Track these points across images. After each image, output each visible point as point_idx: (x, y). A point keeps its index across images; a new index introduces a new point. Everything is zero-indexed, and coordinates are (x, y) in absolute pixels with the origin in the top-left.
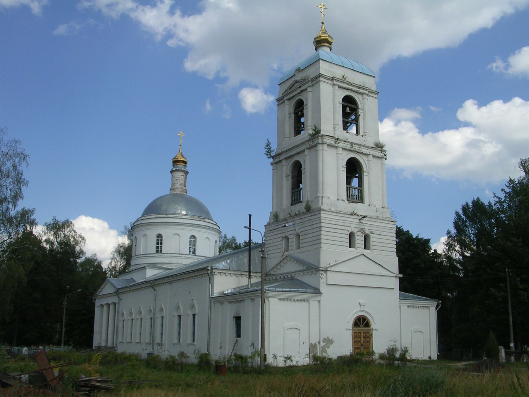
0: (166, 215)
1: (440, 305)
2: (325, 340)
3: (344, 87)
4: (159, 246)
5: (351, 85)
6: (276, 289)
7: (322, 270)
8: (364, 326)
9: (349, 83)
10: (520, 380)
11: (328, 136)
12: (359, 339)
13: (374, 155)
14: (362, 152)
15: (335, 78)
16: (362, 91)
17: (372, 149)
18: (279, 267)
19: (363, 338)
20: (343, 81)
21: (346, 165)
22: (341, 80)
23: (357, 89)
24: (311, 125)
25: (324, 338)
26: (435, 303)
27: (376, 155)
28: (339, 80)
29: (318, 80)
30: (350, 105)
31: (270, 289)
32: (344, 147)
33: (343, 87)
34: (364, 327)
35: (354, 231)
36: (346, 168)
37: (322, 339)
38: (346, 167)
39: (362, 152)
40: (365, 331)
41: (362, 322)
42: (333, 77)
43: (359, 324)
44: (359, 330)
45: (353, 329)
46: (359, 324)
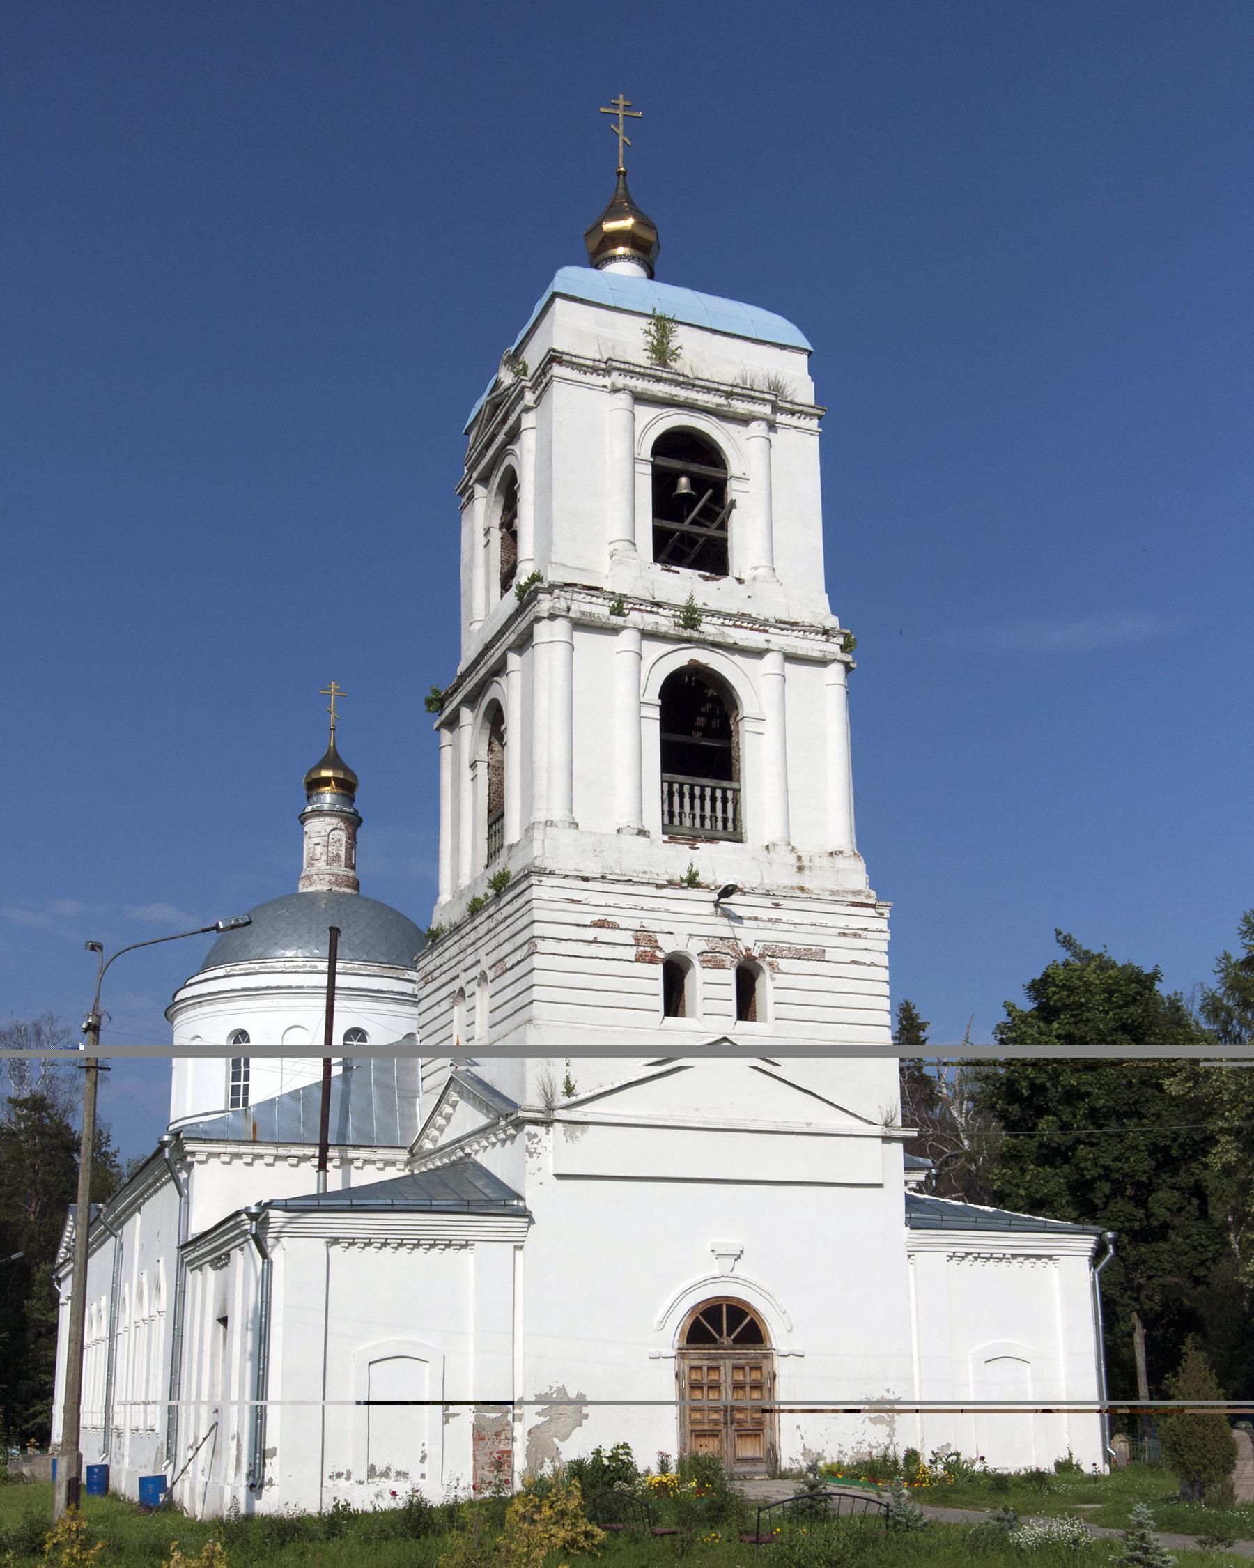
0: (263, 965)
3: (660, 394)
4: (242, 1083)
5: (694, 386)
6: (355, 1202)
7: (535, 1122)
8: (736, 1341)
9: (681, 379)
10: (60, 1494)
13: (791, 650)
14: (731, 641)
15: (615, 364)
16: (741, 407)
17: (782, 629)
18: (440, 1121)
19: (730, 1392)
20: (653, 372)
21: (659, 698)
22: (642, 370)
23: (722, 401)
24: (532, 557)
26: (1087, 1243)
28: (637, 370)
29: (548, 376)
30: (695, 468)
31: (322, 1202)
32: (648, 628)
34: (739, 1346)
36: (661, 707)
38: (659, 702)
40: (743, 1361)
41: (725, 1326)
42: (610, 359)
44: (711, 1357)
45: (682, 1355)
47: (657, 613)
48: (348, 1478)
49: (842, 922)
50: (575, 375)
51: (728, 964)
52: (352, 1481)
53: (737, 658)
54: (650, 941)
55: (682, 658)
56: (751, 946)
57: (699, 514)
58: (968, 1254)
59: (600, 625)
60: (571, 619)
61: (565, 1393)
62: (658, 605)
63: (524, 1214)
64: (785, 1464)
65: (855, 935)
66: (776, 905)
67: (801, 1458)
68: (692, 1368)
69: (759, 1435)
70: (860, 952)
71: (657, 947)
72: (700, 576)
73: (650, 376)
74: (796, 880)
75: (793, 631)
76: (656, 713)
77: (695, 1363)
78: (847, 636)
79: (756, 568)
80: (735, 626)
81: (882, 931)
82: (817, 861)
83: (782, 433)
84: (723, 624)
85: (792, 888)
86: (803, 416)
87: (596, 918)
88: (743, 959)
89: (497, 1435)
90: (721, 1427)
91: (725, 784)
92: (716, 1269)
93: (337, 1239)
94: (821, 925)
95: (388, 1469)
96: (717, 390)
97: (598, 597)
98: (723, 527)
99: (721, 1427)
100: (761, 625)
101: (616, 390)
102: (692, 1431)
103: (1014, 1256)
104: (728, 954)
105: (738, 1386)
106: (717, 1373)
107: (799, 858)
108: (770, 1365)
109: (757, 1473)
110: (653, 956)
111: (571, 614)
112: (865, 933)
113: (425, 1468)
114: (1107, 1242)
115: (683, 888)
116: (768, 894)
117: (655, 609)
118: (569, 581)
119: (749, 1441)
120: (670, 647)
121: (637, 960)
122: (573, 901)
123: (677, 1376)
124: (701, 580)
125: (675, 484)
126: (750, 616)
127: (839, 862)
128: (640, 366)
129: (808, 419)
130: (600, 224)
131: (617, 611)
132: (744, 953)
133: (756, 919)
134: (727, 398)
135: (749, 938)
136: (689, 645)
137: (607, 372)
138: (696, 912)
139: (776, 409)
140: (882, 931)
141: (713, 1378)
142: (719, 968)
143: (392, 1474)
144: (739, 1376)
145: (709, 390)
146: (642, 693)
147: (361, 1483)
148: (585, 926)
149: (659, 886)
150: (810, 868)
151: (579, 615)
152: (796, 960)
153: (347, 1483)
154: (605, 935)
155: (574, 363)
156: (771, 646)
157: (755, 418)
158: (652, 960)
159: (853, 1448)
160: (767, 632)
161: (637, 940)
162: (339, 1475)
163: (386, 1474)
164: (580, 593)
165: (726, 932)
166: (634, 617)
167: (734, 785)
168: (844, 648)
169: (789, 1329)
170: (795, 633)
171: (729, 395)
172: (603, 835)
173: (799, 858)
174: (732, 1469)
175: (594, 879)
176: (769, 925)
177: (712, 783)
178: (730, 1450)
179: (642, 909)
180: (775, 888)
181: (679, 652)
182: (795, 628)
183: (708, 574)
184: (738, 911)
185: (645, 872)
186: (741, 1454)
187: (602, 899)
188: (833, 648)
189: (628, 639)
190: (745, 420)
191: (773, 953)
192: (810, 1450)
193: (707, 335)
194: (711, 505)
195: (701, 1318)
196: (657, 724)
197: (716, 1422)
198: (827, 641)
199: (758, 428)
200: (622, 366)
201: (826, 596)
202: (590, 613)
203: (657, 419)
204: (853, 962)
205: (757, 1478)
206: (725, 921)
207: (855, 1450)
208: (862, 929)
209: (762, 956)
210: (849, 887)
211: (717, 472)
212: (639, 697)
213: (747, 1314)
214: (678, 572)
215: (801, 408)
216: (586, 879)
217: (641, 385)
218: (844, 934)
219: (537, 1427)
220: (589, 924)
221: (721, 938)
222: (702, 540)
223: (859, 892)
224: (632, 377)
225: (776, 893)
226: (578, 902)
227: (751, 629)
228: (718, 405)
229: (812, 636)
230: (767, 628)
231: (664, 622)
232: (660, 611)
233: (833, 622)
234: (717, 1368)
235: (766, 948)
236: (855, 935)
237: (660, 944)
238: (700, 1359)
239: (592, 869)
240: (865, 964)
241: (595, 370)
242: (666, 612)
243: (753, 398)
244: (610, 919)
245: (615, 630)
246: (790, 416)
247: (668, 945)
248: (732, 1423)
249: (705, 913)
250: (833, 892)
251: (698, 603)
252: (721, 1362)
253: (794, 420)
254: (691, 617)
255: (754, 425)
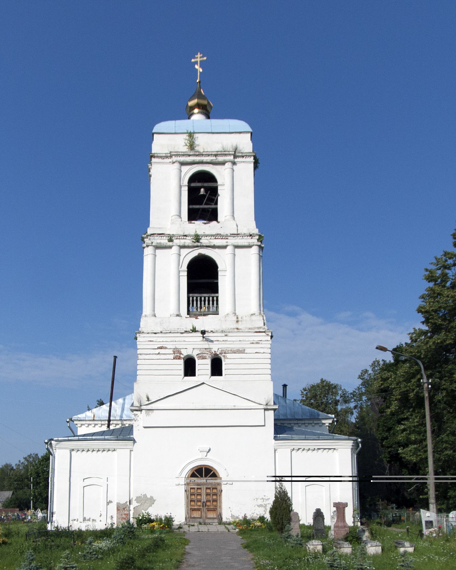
1: (360, 445)
2: (138, 499)
3: (189, 161)
5: (203, 155)
11: (155, 234)
12: (199, 497)
13: (236, 244)
16: (221, 159)
17: (234, 237)
19: (205, 496)
23: (214, 158)
25: (152, 497)
26: (350, 443)
27: (240, 244)
28: (181, 154)
30: (206, 185)
32: (181, 244)
33: (187, 162)
35: (188, 354)
37: (133, 496)
39: (214, 245)
40: (210, 486)
43: (209, 475)
46: (209, 475)
47: (186, 239)
48: (77, 521)
49: (251, 339)
50: (160, 160)
51: (207, 357)
52: (78, 522)
53: (217, 250)
54: (179, 352)
55: (195, 253)
56: (216, 350)
57: (206, 200)
58: (299, 449)
59: (165, 246)
60: (154, 246)
61: (146, 496)
62: (186, 236)
63: (134, 441)
64: (224, 520)
65: (257, 343)
66: (226, 335)
67: (230, 518)
68: (191, 488)
69: (215, 510)
70: (259, 349)
71: (181, 354)
72: (203, 223)
73: (186, 155)
74: (236, 326)
75: (238, 237)
76: (186, 274)
77: (192, 487)
78: (260, 236)
79: (226, 217)
80: (215, 238)
81: (268, 341)
82: (244, 318)
83: (238, 165)
84: (211, 239)
85: (234, 329)
86: (247, 157)
87: (159, 346)
88: (213, 355)
89: (124, 509)
90: (201, 507)
91: (213, 295)
92: (200, 455)
93: (73, 449)
94: (243, 341)
95: (90, 518)
96: (212, 155)
97: (164, 237)
98: (216, 203)
99: (201, 507)
100: (225, 237)
101: (174, 163)
102: (191, 509)
103: (319, 449)
104: (208, 354)
105: (207, 494)
106: (200, 490)
107: (237, 318)
108: (220, 487)
109: (214, 523)
110: (180, 357)
111: (153, 244)
112: (261, 342)
113: (101, 518)
114: (359, 443)
115: (191, 333)
116: (222, 332)
117: (185, 237)
118: (152, 233)
119: (211, 512)
120: (191, 250)
121: (174, 359)
122: (151, 341)
123: (186, 491)
124: (203, 224)
125: (199, 191)
126: (220, 234)
127: (254, 318)
128: (182, 152)
129: (249, 157)
130: (188, 104)
131: (171, 240)
132: (214, 353)
133: (218, 341)
134: (216, 156)
135: (215, 348)
136: (198, 248)
137: (171, 157)
138: (195, 341)
139: (235, 157)
140: (268, 341)
141: (199, 491)
142: (204, 359)
143: (91, 520)
144: (208, 491)
145: (209, 155)
146: (180, 267)
147: (81, 522)
148: (156, 349)
149: (181, 333)
150: (241, 321)
151: (156, 244)
152: (234, 354)
153: (77, 522)
154: (162, 351)
155: (159, 156)
156: (228, 244)
157: (226, 162)
158: (180, 358)
159: (250, 515)
160: (227, 239)
161: (174, 352)
162: (75, 520)
163: (89, 520)
164: (157, 236)
165: (207, 346)
166: (176, 242)
167: (216, 295)
168: (258, 240)
169: (227, 475)
170: (239, 238)
171: (216, 155)
172: (164, 318)
173: (237, 318)
174: (205, 521)
175: (158, 333)
176: (223, 342)
177: (208, 295)
178: (205, 515)
179: (175, 341)
180: (227, 329)
181: (194, 251)
182: (238, 236)
183: (206, 222)
184: (212, 339)
185: (178, 329)
186: (208, 516)
187: (161, 339)
188: (254, 240)
189: (175, 249)
190: (223, 163)
191: (225, 352)
192: (234, 516)
193: (210, 135)
194: (211, 197)
195: (195, 472)
196: (186, 278)
197: (200, 506)
198: (252, 238)
199: (228, 165)
200: (175, 154)
201: (254, 222)
202: (160, 243)
203: (189, 170)
204: (256, 353)
205: (214, 524)
206: (206, 342)
207: (251, 516)
208: (260, 341)
209: (221, 353)
210: (257, 326)
211: (214, 184)
212: (179, 269)
213: (212, 471)
214: (194, 223)
215: (246, 154)
216: (155, 333)
217: (182, 159)
218: (253, 343)
219: (137, 506)
220: (184, 332)
221: (205, 349)
222: (210, 210)
223: (260, 328)
224: (180, 157)
225: (226, 331)
226: (153, 341)
227: (222, 239)
228: (212, 160)
229: (246, 237)
230: (228, 237)
231: (188, 241)
232: (187, 238)
233: (256, 231)
234: (200, 489)
235: (222, 351)
236: (257, 343)
237: (182, 353)
238: (194, 485)
239: (158, 330)
240: (261, 353)
241: (167, 157)
242: (189, 238)
243: (226, 154)
244: (164, 346)
245: (170, 247)
246: (242, 158)
247: (185, 353)
248: (205, 506)
249: (199, 340)
250: (250, 329)
251: (199, 233)
252: (202, 487)
253: (244, 159)
254: (197, 238)
255: (227, 164)
